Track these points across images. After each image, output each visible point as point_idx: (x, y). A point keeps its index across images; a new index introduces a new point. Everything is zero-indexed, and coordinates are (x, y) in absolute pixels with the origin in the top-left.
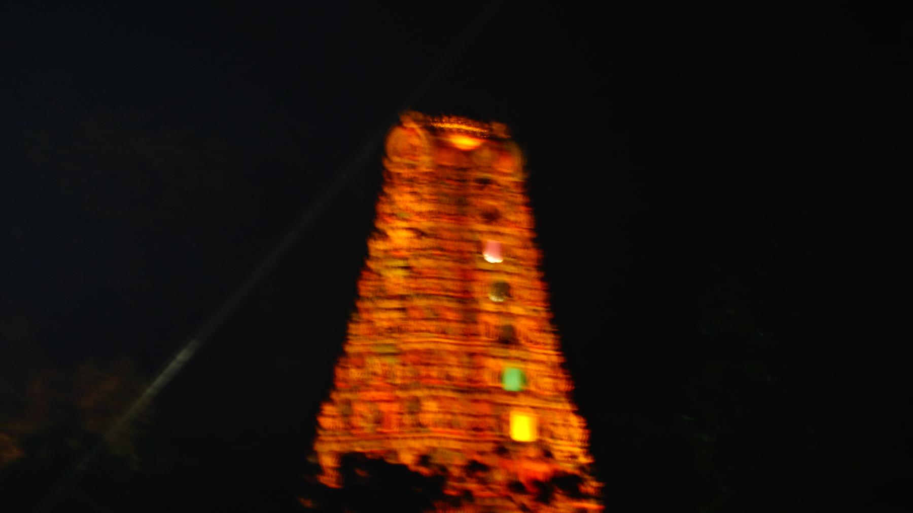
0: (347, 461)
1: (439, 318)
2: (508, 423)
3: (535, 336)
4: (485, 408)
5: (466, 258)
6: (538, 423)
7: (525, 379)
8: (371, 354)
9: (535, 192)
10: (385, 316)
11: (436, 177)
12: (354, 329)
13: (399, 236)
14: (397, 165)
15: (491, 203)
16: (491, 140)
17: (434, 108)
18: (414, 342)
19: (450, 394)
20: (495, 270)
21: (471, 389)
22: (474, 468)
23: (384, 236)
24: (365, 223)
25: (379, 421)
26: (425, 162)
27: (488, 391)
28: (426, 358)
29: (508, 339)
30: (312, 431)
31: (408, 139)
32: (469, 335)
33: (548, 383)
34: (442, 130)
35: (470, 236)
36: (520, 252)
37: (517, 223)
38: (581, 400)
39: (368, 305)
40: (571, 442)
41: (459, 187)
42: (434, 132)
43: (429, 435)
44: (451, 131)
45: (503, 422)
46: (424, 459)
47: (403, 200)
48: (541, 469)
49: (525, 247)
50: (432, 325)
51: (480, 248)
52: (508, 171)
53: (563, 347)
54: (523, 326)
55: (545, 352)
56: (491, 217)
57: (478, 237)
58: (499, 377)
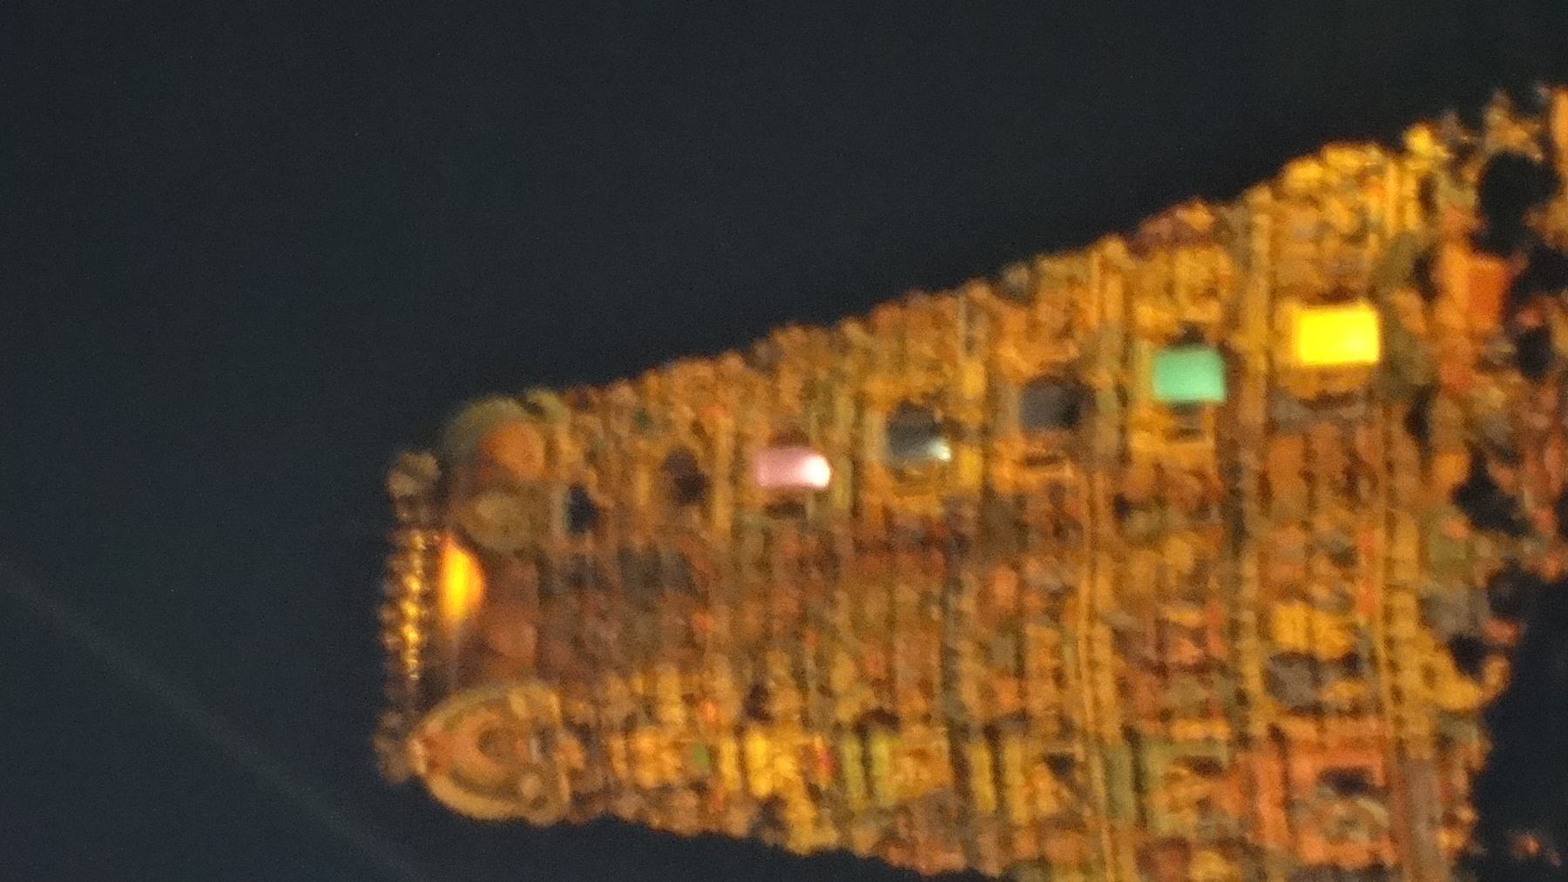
1: (1011, 624)
2: (1325, 374)
3: (1047, 313)
4: (1286, 454)
5: (826, 550)
6: (1323, 285)
7: (1189, 337)
8: (1143, 818)
9: (599, 352)
11: (574, 667)
13: (771, 762)
14: (545, 793)
15: (643, 487)
17: (353, 680)
18: (1096, 697)
19: (1249, 568)
20: (854, 467)
21: (1228, 509)
22: (1481, 501)
23: (771, 809)
25: (1348, 783)
26: (533, 700)
27: (1228, 448)
28: (1143, 654)
29: (1065, 403)
31: (454, 759)
32: (1061, 528)
33: (1189, 265)
34: (426, 650)
35: (752, 544)
36: (790, 384)
37: (699, 398)
38: (1238, 164)
39: (987, 843)
41: (601, 592)
42: (432, 692)
44: (428, 625)
45: (1329, 396)
46: (1467, 654)
47: (653, 758)
49: (771, 370)
50: (1038, 632)
51: (789, 504)
52: (536, 439)
53: (1077, 236)
54: (1021, 360)
55: (1097, 285)
56: (688, 485)
57: (752, 518)
58: (1184, 415)
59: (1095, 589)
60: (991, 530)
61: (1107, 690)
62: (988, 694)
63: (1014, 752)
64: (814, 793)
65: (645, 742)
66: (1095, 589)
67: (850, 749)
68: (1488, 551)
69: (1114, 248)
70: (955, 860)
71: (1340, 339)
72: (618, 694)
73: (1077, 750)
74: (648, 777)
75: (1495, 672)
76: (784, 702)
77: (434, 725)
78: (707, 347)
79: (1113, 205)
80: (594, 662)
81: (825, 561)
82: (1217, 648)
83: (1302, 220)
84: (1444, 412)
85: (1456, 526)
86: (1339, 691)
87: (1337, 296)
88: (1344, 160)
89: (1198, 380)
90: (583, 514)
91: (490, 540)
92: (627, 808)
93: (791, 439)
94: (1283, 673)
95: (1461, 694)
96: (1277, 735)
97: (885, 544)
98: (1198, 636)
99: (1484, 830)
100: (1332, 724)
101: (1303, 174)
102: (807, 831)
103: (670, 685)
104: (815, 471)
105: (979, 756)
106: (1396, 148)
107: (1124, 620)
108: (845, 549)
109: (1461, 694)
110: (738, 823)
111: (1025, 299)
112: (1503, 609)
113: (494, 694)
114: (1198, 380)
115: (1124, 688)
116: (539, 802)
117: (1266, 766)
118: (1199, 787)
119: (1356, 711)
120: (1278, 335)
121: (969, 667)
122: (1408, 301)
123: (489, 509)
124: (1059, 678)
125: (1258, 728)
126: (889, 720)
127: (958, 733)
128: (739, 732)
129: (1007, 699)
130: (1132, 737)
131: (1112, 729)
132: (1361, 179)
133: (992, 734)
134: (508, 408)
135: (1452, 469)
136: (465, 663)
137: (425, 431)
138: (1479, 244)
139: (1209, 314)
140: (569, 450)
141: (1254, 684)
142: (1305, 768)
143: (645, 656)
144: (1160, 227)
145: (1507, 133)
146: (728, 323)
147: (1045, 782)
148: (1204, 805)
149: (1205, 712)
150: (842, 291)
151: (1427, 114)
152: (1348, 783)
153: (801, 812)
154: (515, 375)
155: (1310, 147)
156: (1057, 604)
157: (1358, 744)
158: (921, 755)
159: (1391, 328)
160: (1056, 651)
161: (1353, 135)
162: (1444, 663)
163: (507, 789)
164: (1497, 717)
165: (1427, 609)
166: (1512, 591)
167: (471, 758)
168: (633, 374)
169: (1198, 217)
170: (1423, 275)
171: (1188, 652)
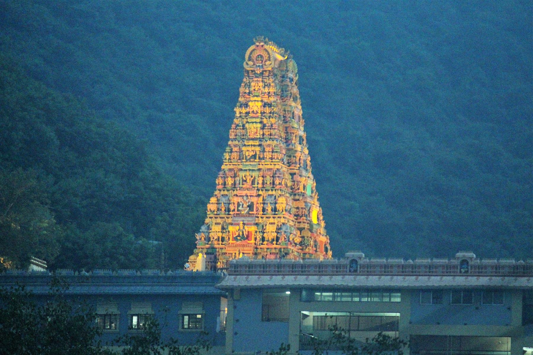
13: (255, 106)
18: (266, 165)
61: (269, 167)
62: (269, 145)
63: (258, 149)
64: (248, 113)
65: (261, 84)
67: (258, 120)
70: (232, 137)
73: (257, 160)
74: (253, 84)
76: (267, 110)
82: (278, 187)
86: (269, 208)
94: (273, 198)
96: (259, 196)
98: (280, 184)
100: (262, 205)
103: (272, 90)
105: (257, 143)
108: (287, 125)
115: (270, 169)
116: (247, 64)
117: (254, 192)
119: (264, 210)
124: (272, 159)
125: (260, 192)
127: (260, 140)
128: (262, 101)
129: (267, 149)
130: (259, 170)
131: (261, 167)
133: (260, 145)
141: (270, 192)
142: (254, 200)
147: (252, 153)
152: (251, 207)
160: (278, 158)
163: (250, 59)
167: (257, 53)
171: (277, 182)
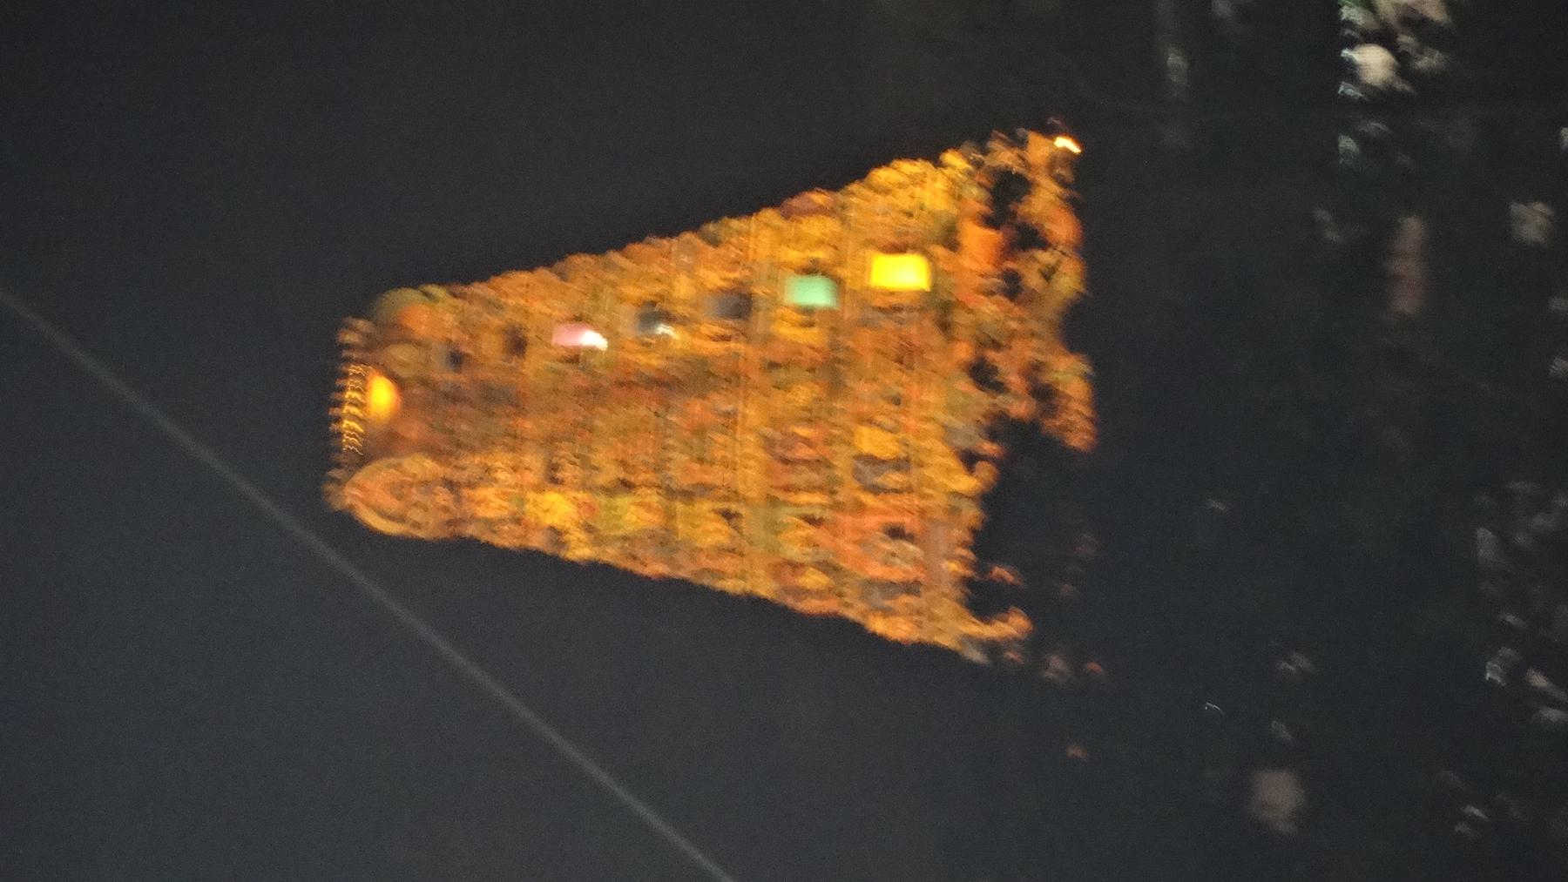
0: (982, 599)
1: (700, 431)
5: (595, 386)
6: (890, 244)
9: (464, 266)
10: (705, 529)
12: (731, 585)
13: (557, 509)
14: (426, 523)
16: (373, 353)
17: (316, 450)
18: (751, 478)
21: (832, 370)
22: (982, 374)
23: (556, 533)
24: (540, 570)
25: (896, 533)
26: (422, 466)
28: (780, 455)
29: (740, 305)
30: (925, 656)
31: (376, 499)
33: (812, 225)
37: (525, 294)
38: (845, 167)
40: (926, 186)
41: (465, 405)
42: (363, 459)
43: (925, 450)
45: (893, 307)
46: (969, 460)
48: (979, 241)
51: (575, 358)
52: (429, 314)
53: (748, 208)
54: (715, 278)
55: (761, 237)
56: (517, 344)
58: (808, 315)
59: (752, 413)
60: (695, 377)
66: (752, 413)
68: (982, 401)
69: (769, 215)
71: (904, 274)
72: (471, 464)
75: (985, 471)
76: (568, 473)
77: (360, 477)
78: (528, 262)
79: (769, 188)
80: (459, 445)
81: (593, 394)
83: (881, 201)
84: (961, 318)
85: (964, 385)
86: (893, 479)
87: (897, 249)
88: (908, 168)
89: (816, 294)
90: (457, 360)
91: (404, 373)
92: (471, 530)
93: (580, 319)
95: (966, 483)
97: (631, 383)
99: (977, 567)
101: (882, 175)
102: (580, 550)
104: (592, 339)
106: (938, 164)
107: (768, 431)
109: (966, 483)
110: (537, 541)
111: (715, 242)
112: (992, 435)
113: (393, 461)
114: (816, 294)
118: (810, 531)
120: (865, 269)
121: (680, 458)
122: (940, 251)
123: (400, 354)
126: (627, 486)
132: (918, 181)
134: (410, 295)
135: (964, 351)
136: (382, 444)
137: (362, 309)
138: (989, 222)
139: (821, 254)
140: (450, 319)
143: (487, 443)
144: (795, 202)
145: (1004, 157)
146: (542, 250)
148: (809, 542)
149: (811, 488)
150: (610, 235)
151: (955, 145)
152: (896, 533)
153: (576, 536)
154: (416, 279)
155: (885, 161)
156: (729, 421)
157: (902, 511)
158: (648, 507)
159: (936, 273)
161: (912, 156)
162: (953, 463)
164: (988, 500)
165: (947, 433)
166: (998, 426)
168: (483, 278)
169: (819, 198)
170: (950, 237)
